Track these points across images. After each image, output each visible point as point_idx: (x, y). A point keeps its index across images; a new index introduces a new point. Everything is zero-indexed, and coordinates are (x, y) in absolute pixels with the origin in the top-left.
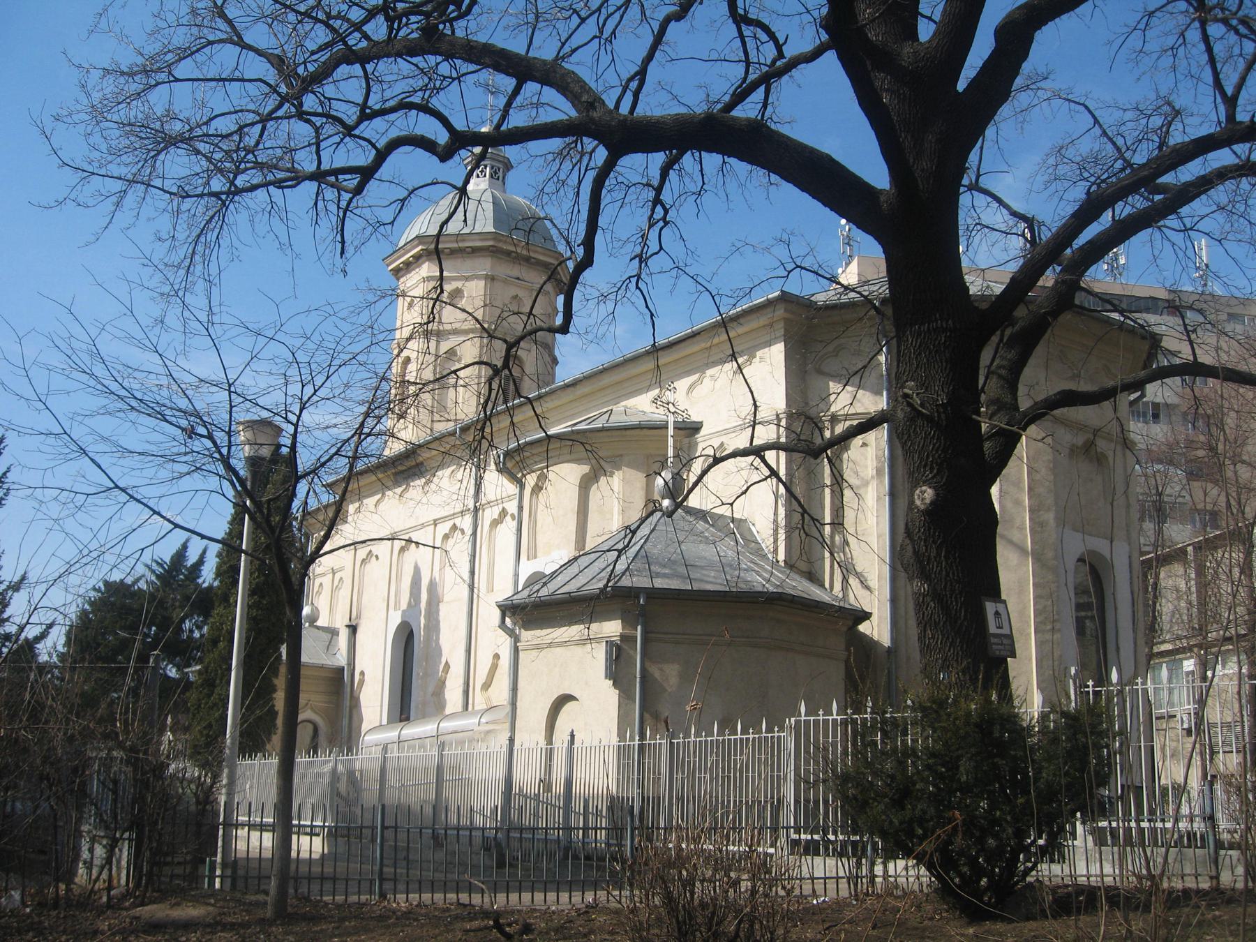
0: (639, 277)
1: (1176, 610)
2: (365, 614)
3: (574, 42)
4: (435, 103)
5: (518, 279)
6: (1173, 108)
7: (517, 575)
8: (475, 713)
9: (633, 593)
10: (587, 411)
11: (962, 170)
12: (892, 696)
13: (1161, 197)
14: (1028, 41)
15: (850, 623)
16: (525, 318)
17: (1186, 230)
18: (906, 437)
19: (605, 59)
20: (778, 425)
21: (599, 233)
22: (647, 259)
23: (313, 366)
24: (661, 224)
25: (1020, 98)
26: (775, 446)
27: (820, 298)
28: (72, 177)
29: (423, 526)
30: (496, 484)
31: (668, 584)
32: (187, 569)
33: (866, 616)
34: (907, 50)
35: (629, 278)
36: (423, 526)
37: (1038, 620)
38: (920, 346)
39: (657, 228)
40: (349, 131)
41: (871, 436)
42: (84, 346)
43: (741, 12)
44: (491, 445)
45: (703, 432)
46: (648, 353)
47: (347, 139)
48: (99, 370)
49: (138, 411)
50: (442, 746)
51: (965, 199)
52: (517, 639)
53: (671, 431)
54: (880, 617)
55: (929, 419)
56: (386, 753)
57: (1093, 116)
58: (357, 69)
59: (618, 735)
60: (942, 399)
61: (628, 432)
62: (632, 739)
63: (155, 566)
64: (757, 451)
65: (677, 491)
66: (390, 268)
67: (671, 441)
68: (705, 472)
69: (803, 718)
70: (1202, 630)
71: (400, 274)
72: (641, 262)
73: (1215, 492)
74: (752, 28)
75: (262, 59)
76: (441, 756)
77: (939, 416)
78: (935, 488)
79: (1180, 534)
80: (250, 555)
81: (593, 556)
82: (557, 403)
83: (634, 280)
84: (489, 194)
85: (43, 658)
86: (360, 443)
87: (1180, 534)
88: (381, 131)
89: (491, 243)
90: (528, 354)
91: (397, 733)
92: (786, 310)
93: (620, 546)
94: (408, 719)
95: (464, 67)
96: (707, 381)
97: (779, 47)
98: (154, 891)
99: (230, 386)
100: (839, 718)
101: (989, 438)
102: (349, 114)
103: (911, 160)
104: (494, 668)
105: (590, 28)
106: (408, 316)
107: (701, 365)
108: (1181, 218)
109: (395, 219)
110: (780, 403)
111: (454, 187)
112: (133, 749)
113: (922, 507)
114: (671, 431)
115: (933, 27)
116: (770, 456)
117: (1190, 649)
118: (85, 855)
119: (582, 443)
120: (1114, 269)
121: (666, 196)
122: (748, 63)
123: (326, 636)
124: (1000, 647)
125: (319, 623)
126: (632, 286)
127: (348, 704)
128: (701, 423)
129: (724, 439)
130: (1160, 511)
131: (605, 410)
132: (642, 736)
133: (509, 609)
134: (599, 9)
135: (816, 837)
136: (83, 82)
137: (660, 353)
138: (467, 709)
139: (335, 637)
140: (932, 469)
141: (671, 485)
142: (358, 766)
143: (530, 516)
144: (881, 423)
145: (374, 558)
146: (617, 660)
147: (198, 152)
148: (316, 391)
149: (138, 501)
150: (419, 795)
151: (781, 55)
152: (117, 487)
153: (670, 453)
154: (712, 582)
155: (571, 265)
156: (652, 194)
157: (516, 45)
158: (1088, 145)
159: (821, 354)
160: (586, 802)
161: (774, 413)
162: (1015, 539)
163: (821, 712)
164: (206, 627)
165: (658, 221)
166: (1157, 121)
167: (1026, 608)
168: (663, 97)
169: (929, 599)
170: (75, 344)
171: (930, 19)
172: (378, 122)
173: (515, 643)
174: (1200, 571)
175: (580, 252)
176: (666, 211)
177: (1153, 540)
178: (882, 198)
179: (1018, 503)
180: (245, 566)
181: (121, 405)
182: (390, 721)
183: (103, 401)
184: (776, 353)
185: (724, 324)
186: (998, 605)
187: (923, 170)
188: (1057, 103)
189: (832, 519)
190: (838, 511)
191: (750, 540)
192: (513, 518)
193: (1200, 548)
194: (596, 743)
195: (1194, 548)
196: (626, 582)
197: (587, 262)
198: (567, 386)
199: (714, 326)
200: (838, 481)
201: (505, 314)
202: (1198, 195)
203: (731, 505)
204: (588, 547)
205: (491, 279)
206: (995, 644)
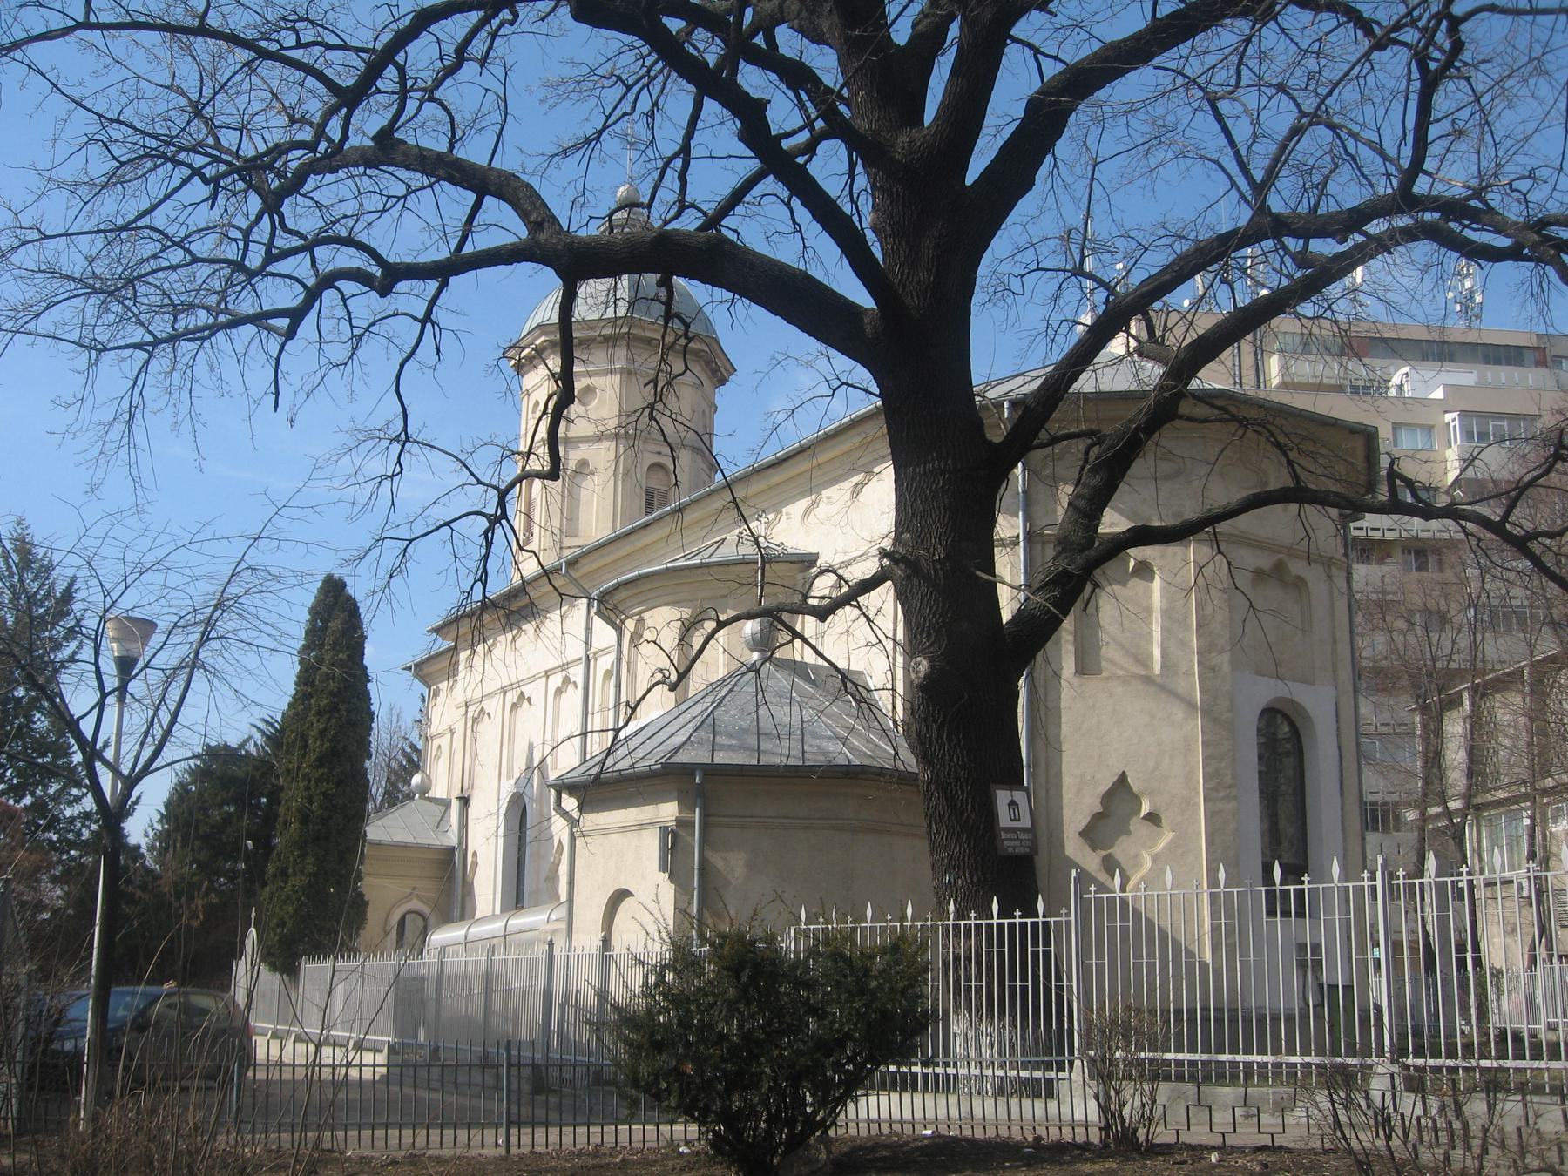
9: (687, 770)
29: (534, 678)
31: (731, 758)
36: (534, 678)
37: (1207, 786)
60: (940, 554)
61: (731, 568)
63: (262, 725)
78: (930, 660)
91: (463, 932)
107: (811, 486)
111: (415, 319)
123: (438, 810)
124: (1014, 843)
125: (431, 794)
140: (929, 636)
144: (883, 581)
162: (1180, 690)
163: (1018, 913)
167: (1193, 771)
169: (933, 787)
176: (687, 326)
178: (866, 320)
179: (1183, 644)
182: (502, 911)
186: (1016, 793)
196: (681, 758)
206: (1006, 840)
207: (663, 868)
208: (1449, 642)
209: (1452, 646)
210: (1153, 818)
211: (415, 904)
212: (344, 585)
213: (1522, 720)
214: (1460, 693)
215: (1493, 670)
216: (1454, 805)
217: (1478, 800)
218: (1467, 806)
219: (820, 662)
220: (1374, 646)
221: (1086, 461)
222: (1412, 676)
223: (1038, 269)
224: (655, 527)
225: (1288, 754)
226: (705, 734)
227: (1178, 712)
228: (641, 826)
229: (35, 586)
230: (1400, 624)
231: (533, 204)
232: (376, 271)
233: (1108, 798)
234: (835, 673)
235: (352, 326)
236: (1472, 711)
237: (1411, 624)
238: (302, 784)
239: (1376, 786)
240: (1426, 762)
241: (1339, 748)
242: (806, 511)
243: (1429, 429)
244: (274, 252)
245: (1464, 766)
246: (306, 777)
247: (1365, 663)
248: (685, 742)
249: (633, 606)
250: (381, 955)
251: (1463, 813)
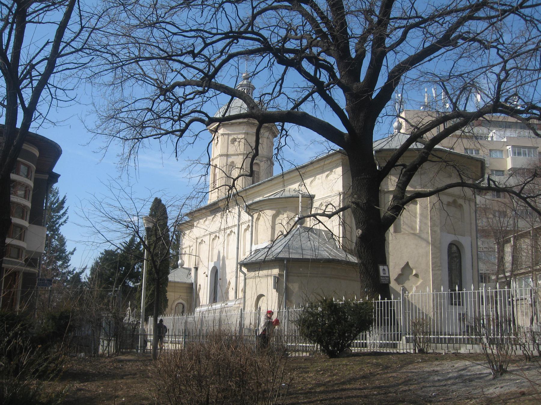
9: (282, 260)
10: (277, 189)
21: (260, 145)
24: (285, 136)
30: (245, 217)
32: (136, 245)
45: (315, 199)
60: (365, 201)
63: (124, 244)
67: (300, 204)
69: (392, 300)
78: (362, 230)
82: (266, 186)
85: (83, 280)
94: (216, 302)
96: (317, 179)
112: (114, 313)
118: (101, 343)
123: (187, 271)
140: (362, 223)
146: (277, 282)
154: (308, 255)
157: (231, 85)
163: (386, 299)
167: (428, 262)
169: (362, 265)
176: (287, 132)
178: (345, 137)
179: (426, 224)
196: (281, 256)
207: (275, 288)
208: (506, 222)
209: (508, 222)
210: (416, 275)
211: (180, 301)
212: (161, 201)
213: (530, 247)
214: (510, 238)
215: (520, 231)
216: (508, 274)
217: (516, 273)
218: (511, 274)
219: (326, 229)
220: (483, 223)
221: (401, 173)
222: (494, 233)
223: (387, 115)
224: (262, 185)
225: (456, 257)
226: (287, 249)
227: (424, 244)
228: (267, 276)
229: (53, 199)
230: (491, 216)
231: (250, 101)
232: (207, 119)
233: (403, 269)
234: (329, 232)
235: (180, 127)
236: (514, 244)
237: (495, 216)
239: (483, 268)
240: (499, 260)
241: (472, 256)
242: (311, 181)
243: (502, 151)
244: (181, 115)
245: (511, 262)
247: (479, 228)
248: (281, 251)
250: (169, 315)
251: (510, 277)
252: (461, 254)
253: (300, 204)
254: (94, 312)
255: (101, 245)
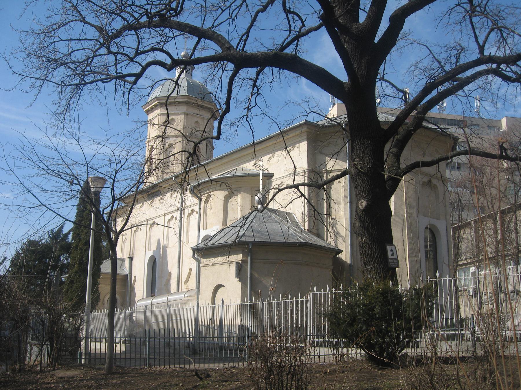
0: (247, 115)
1: (468, 247)
2: (136, 253)
3: (219, 20)
4: (166, 48)
5: (198, 114)
6: (461, 46)
7: (199, 236)
8: (182, 293)
9: (247, 243)
11: (377, 73)
12: (349, 283)
13: (456, 83)
14: (403, 22)
15: (334, 254)
16: (202, 133)
17: (467, 96)
18: (355, 180)
19: (232, 27)
20: (305, 176)
21: (232, 99)
22: (251, 109)
23: (121, 156)
24: (256, 94)
25: (400, 43)
26: (304, 184)
27: (321, 123)
28: (18, 78)
29: (160, 216)
30: (190, 200)
33: (340, 251)
34: (355, 26)
35: (243, 116)
36: (160, 216)
38: (360, 144)
39: (254, 96)
40: (131, 60)
41: (342, 179)
42: (29, 149)
43: (288, 8)
44: (188, 184)
45: (274, 177)
46: (251, 145)
47: (131, 63)
48: (35, 158)
49: (51, 175)
50: (169, 306)
51: (378, 84)
52: (199, 262)
53: (261, 177)
54: (346, 252)
55: (364, 173)
56: (170, 308)
57: (430, 50)
58: (133, 32)
59: (241, 300)
60: (369, 165)
62: (247, 302)
64: (296, 186)
65: (263, 201)
66: (145, 110)
67: (261, 181)
68: (275, 195)
70: (477, 255)
71: (149, 113)
72: (248, 110)
73: (482, 199)
74: (292, 15)
75: (93, 28)
76: (169, 310)
77: (368, 172)
78: (367, 201)
79: (469, 216)
80: (94, 230)
81: (230, 228)
82: (214, 166)
83: (245, 117)
84: (185, 79)
86: (138, 187)
87: (469, 216)
88: (144, 59)
89: (186, 100)
90: (203, 146)
91: (151, 301)
92: (307, 128)
93: (241, 224)
95: (175, 32)
96: (275, 156)
97: (303, 22)
98: (58, 365)
99: (87, 164)
100: (329, 292)
101: (388, 181)
102: (132, 54)
103: (356, 70)
104: (190, 274)
105: (226, 15)
106: (153, 132)
107: (273, 151)
108: (464, 91)
109: (149, 94)
110: (306, 166)
113: (362, 208)
114: (261, 177)
115: (365, 15)
116: (301, 188)
117: (473, 263)
119: (225, 183)
120: (441, 108)
121: (257, 84)
122: (290, 30)
126: (245, 119)
127: (129, 290)
128: (273, 174)
129: (283, 180)
130: (460, 207)
131: (234, 169)
132: (251, 301)
133: (195, 250)
134: (230, 7)
135: (321, 340)
136: (21, 39)
137: (256, 146)
138: (179, 291)
139: (123, 262)
141: (261, 200)
142: (134, 315)
143: (204, 212)
145: (139, 230)
147: (69, 67)
148: (122, 166)
149: (51, 210)
150: (160, 326)
151: (303, 26)
152: (42, 205)
153: (261, 187)
155: (221, 112)
156: (252, 83)
157: (197, 23)
158: (427, 62)
159: (322, 145)
160: (229, 329)
161: (303, 169)
164: (69, 259)
165: (255, 93)
166: (454, 52)
168: (257, 44)
170: (26, 148)
171: (364, 10)
172: (143, 56)
173: (199, 264)
174: (476, 231)
175: (224, 107)
176: (258, 90)
177: (457, 219)
178: (345, 86)
180: (92, 235)
181: (44, 172)
183: (36, 171)
184: (303, 146)
185: (282, 134)
186: (392, 247)
187: (361, 74)
188: (415, 45)
189: (327, 212)
190: (329, 208)
191: (294, 221)
192: (197, 213)
193: (476, 222)
194: (232, 304)
195: (474, 222)
196: (243, 239)
197: (227, 111)
198: (219, 159)
199: (278, 135)
200: (329, 198)
201: (194, 131)
202: (471, 82)
203: (286, 207)
204: (228, 224)
205: (186, 114)
228: (229, 262)
238: (79, 251)
244: (139, 51)
246: (81, 249)
249: (206, 190)
252: (437, 239)
253: (261, 181)
254: (19, 307)
255: (32, 210)
